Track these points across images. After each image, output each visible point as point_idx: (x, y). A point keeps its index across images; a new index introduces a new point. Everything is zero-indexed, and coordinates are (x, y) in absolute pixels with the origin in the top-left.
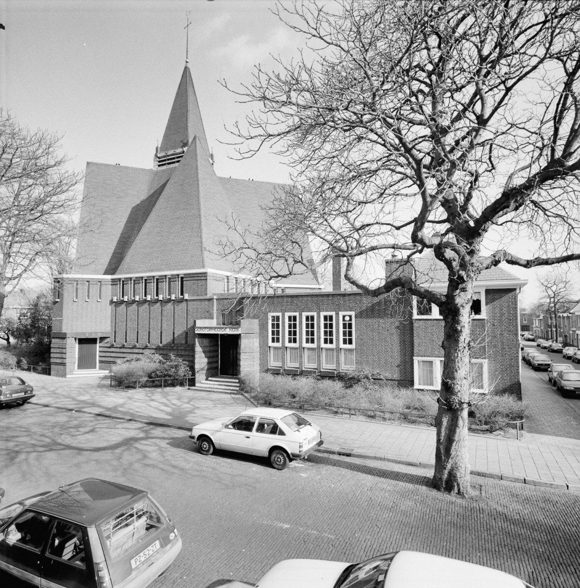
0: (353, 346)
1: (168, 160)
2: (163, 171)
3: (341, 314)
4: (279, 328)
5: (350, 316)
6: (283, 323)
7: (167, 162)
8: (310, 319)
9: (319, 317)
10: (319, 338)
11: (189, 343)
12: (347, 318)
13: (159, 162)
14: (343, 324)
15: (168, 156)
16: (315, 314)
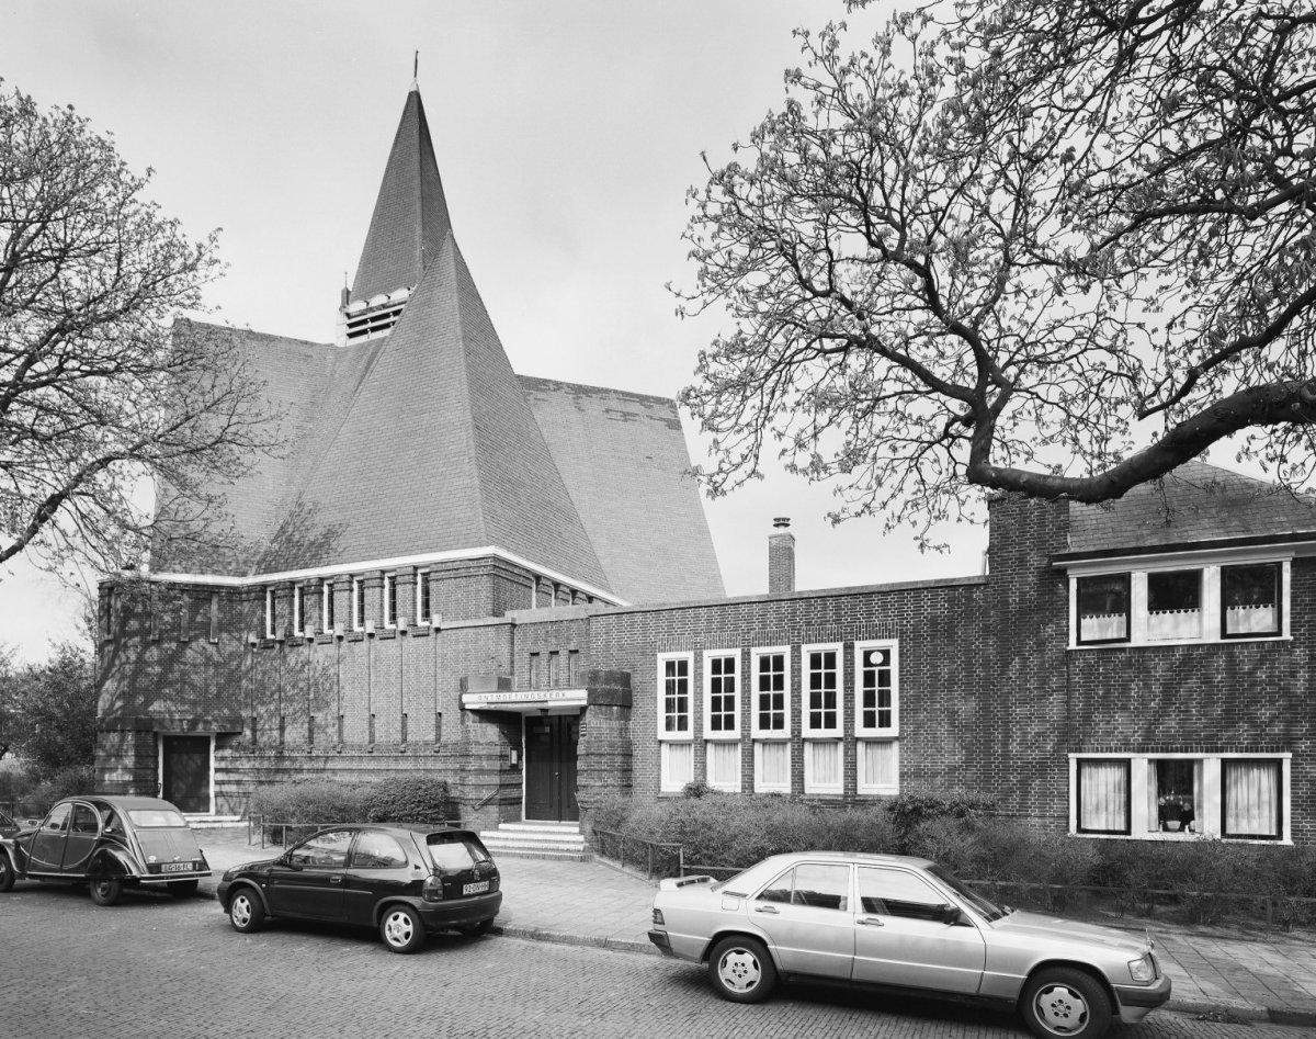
0: (893, 731)
1: (373, 319)
2: (361, 347)
3: (860, 646)
4: (685, 691)
5: (886, 653)
6: (699, 676)
7: (370, 325)
8: (217, 770)
9: (796, 658)
10: (796, 714)
11: (409, 738)
12: (877, 658)
13: (351, 326)
14: (865, 673)
15: (371, 310)
16: (785, 651)
